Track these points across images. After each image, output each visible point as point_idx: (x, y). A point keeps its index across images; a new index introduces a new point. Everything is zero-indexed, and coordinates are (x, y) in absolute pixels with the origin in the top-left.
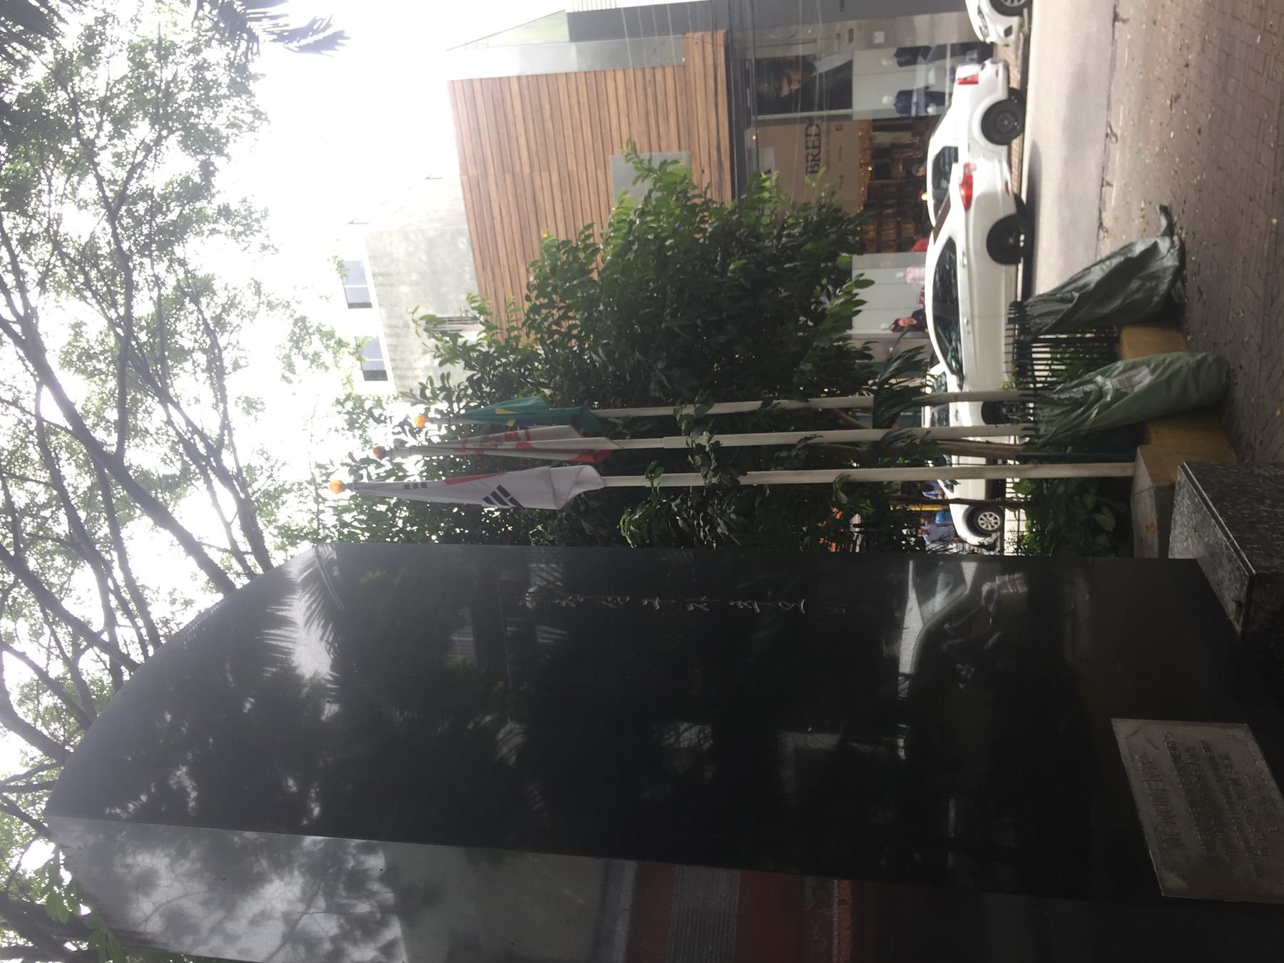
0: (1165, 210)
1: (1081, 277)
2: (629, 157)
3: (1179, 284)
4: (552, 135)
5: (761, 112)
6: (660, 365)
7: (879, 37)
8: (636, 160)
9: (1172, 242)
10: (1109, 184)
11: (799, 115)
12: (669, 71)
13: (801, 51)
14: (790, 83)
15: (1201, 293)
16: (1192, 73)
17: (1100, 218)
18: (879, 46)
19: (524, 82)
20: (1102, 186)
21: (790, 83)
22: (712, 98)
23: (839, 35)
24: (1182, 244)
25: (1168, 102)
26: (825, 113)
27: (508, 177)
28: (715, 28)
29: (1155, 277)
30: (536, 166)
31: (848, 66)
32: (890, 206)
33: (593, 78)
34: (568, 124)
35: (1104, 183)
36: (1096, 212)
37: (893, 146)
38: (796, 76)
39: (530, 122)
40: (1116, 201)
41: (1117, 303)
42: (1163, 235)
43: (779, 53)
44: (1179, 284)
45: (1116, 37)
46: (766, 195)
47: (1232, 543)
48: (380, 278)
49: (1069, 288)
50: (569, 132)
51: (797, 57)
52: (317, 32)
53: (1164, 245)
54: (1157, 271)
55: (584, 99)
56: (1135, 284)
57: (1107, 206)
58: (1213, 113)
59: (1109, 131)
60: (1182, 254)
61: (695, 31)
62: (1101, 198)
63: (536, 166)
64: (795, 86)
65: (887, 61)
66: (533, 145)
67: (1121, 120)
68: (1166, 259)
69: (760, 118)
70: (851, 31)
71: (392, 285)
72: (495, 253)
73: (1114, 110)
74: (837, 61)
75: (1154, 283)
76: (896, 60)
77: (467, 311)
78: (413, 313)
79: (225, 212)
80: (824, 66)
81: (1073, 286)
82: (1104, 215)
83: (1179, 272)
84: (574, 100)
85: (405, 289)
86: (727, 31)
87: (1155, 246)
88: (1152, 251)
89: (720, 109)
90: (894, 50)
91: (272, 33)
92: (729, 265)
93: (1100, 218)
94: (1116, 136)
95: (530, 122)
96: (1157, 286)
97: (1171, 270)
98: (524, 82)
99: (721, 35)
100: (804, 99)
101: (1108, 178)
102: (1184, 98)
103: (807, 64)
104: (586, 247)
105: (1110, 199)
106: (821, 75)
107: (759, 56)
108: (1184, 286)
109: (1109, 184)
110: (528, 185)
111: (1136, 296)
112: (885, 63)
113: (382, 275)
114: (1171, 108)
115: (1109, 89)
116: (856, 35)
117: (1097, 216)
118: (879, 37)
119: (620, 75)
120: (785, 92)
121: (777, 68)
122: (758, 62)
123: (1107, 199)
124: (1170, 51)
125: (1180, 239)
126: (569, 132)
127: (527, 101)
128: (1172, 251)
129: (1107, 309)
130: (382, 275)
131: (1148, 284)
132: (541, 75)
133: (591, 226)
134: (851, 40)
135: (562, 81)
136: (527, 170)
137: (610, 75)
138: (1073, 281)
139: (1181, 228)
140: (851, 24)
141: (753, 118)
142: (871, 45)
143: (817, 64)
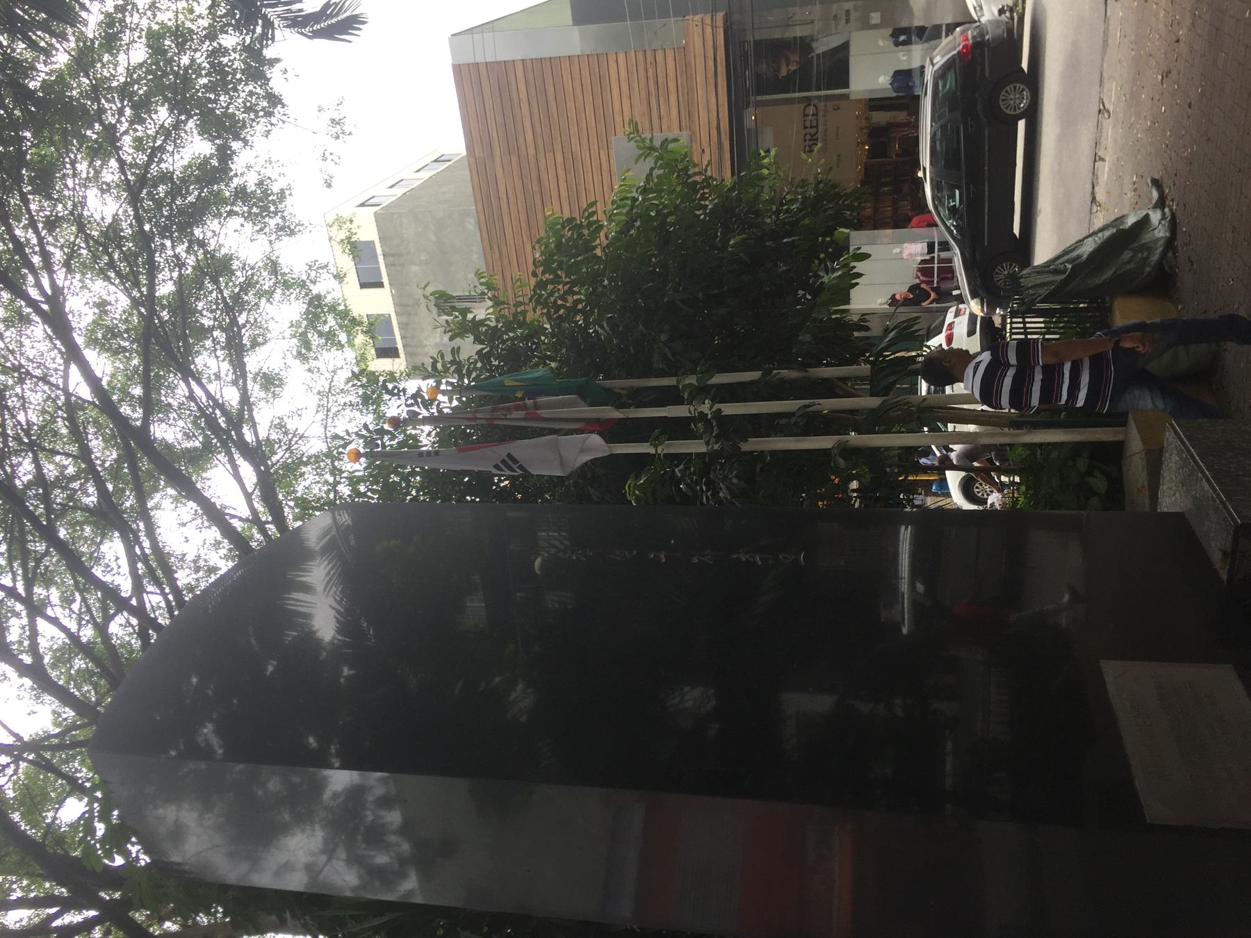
0: (1156, 183)
1: (1074, 249)
2: (632, 136)
3: (1170, 254)
4: (556, 115)
5: (759, 93)
6: (663, 337)
7: (875, 18)
8: (638, 138)
9: (1164, 214)
10: (1102, 159)
11: (797, 95)
12: (670, 54)
13: (798, 32)
14: (788, 65)
15: (1192, 264)
16: (1183, 48)
17: (1093, 193)
18: (876, 27)
19: (529, 65)
20: (1095, 161)
21: (788, 65)
22: (712, 81)
23: (835, 16)
24: (1173, 215)
25: (1160, 77)
26: (823, 93)
27: (514, 158)
28: (714, 11)
29: (1147, 248)
30: (541, 147)
31: (845, 47)
32: (886, 184)
33: (597, 60)
34: (571, 104)
35: (1097, 158)
36: (1089, 187)
37: (890, 126)
38: (795, 57)
39: (534, 105)
40: (1108, 176)
41: (1109, 274)
42: (1155, 207)
43: (777, 35)
44: (1170, 254)
45: (1108, 14)
46: (765, 172)
47: (1218, 495)
48: (391, 258)
49: (1061, 260)
50: (572, 114)
51: (795, 38)
52: (331, 16)
53: (1155, 217)
54: (1149, 243)
55: (587, 82)
56: (1127, 255)
57: (1100, 180)
58: (1203, 87)
59: (1102, 107)
60: (1173, 225)
61: (695, 14)
62: (1094, 173)
63: (541, 147)
64: (793, 68)
65: (882, 41)
66: (537, 125)
67: (1113, 96)
68: (1156, 231)
69: (759, 98)
70: (848, 12)
71: (402, 265)
72: (502, 234)
73: (1106, 86)
74: (834, 42)
75: (1145, 254)
76: (891, 40)
77: (475, 287)
78: (424, 289)
79: (242, 194)
80: (821, 47)
81: (1066, 258)
82: (1096, 189)
83: (1170, 243)
84: (577, 83)
85: (414, 268)
86: (726, 13)
87: (1147, 216)
88: (1144, 222)
89: (720, 90)
90: (890, 31)
91: (286, 19)
92: (729, 240)
93: (1093, 193)
94: (1108, 111)
95: (534, 105)
96: (1147, 258)
97: (1162, 242)
98: (529, 65)
99: (720, 16)
100: (802, 80)
101: (1101, 153)
102: (1174, 72)
103: (804, 45)
104: (590, 224)
105: (1103, 173)
106: (818, 55)
107: (757, 37)
108: (1176, 257)
109: (1102, 159)
110: (533, 165)
111: (1128, 267)
112: (881, 43)
113: (393, 255)
114: (1162, 83)
115: (1102, 66)
116: (853, 15)
117: (1108, 8)
118: (875, 18)
119: (622, 57)
120: (784, 72)
121: (777, 49)
122: (757, 43)
123: (1100, 174)
124: (1161, 26)
125: (1171, 210)
126: (572, 114)
127: (532, 83)
128: (1163, 222)
129: (1098, 280)
130: (393, 255)
131: (1140, 255)
132: (546, 59)
133: (594, 203)
134: (848, 21)
135: (566, 64)
136: (532, 151)
137: (612, 58)
138: (1065, 253)
139: (1172, 200)
140: (847, 6)
141: (752, 98)
142: (867, 26)
143: (814, 45)
